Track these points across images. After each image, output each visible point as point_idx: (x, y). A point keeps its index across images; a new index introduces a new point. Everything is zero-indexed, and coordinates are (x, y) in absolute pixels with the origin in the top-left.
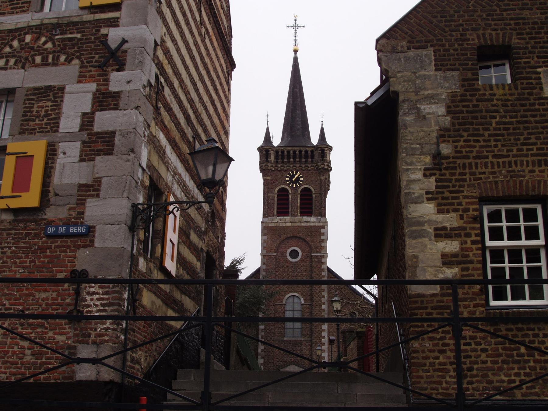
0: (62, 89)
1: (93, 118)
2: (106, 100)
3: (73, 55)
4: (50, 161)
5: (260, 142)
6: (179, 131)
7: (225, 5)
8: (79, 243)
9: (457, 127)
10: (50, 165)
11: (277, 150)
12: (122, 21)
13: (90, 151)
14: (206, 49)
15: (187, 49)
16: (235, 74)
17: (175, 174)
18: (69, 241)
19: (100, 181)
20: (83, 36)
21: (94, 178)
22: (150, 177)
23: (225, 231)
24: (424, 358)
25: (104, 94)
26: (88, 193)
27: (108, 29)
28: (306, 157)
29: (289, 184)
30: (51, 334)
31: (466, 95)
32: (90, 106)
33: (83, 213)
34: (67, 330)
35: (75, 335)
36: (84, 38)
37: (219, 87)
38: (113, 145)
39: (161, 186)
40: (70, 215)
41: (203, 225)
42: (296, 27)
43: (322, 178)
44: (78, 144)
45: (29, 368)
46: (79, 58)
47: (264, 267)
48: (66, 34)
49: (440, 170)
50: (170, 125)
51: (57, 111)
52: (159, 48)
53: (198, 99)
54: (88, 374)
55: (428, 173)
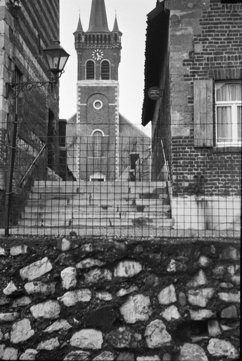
5: (75, 29)
6: (30, 33)
9: (205, 33)
11: (85, 34)
17: (29, 61)
31: (212, 12)
39: (21, 70)
41: (47, 92)
49: (193, 61)
50: (24, 29)
55: (186, 63)
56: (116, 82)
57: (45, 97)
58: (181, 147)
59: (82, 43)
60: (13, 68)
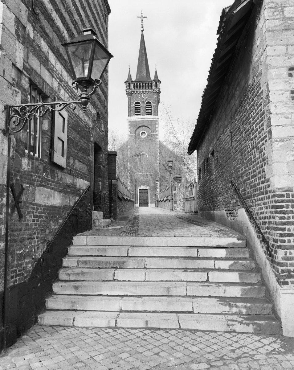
5: (126, 80)
16: (110, 16)
22: (30, 80)
23: (108, 127)
29: (140, 100)
42: (142, 17)
56: (157, 117)
57: (89, 129)
59: (131, 89)
60: (26, 84)
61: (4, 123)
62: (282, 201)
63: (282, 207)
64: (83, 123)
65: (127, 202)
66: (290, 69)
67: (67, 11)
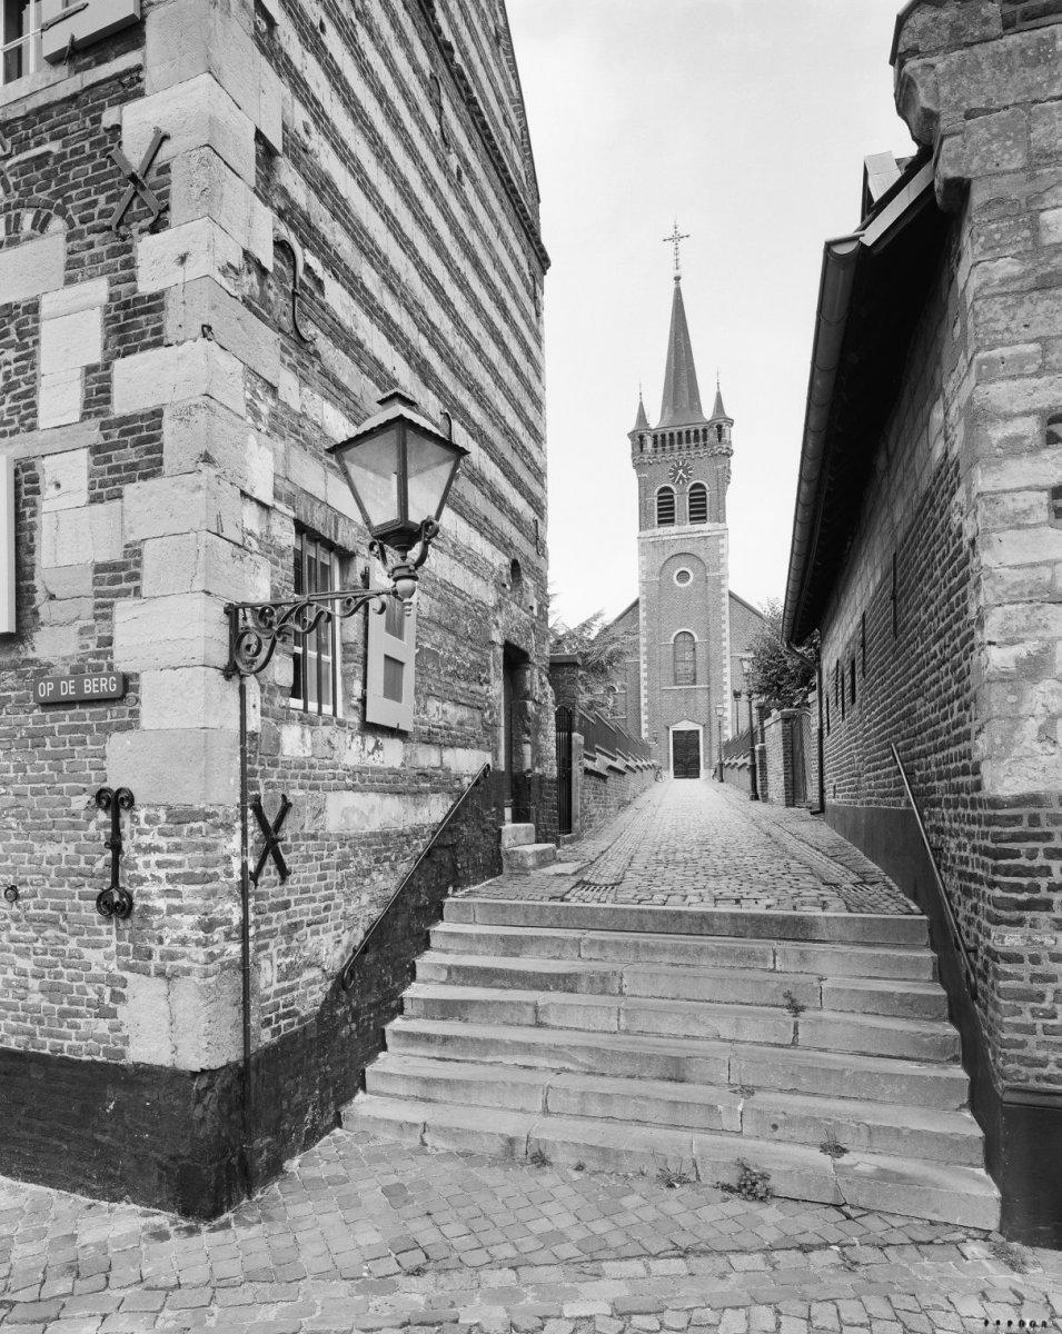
0: (33, 308)
1: (108, 378)
2: (134, 323)
3: (48, 205)
4: (28, 510)
5: (631, 425)
7: (515, 121)
8: (108, 720)
10: (29, 520)
12: (150, 78)
13: (110, 471)
14: (467, 208)
15: (402, 194)
16: (550, 279)
18: (88, 715)
19: (139, 553)
20: (64, 146)
21: (127, 546)
24: (1035, 978)
25: (126, 305)
26: (117, 587)
27: (116, 108)
28: (697, 439)
30: (73, 944)
32: (99, 347)
33: (109, 641)
34: (105, 937)
35: (121, 951)
36: (68, 150)
37: (510, 304)
38: (160, 449)
40: (82, 647)
43: (720, 467)
44: (83, 457)
45: (40, 1022)
46: (62, 212)
47: (644, 597)
48: (27, 148)
51: (30, 373)
52: (284, 163)
53: (451, 325)
54: (154, 1049)
56: (721, 526)
58: (1041, 846)
61: (226, 649)
62: (1015, 838)
63: (1016, 854)
64: (464, 600)
65: (629, 775)
66: (1052, 421)
67: (405, 305)
